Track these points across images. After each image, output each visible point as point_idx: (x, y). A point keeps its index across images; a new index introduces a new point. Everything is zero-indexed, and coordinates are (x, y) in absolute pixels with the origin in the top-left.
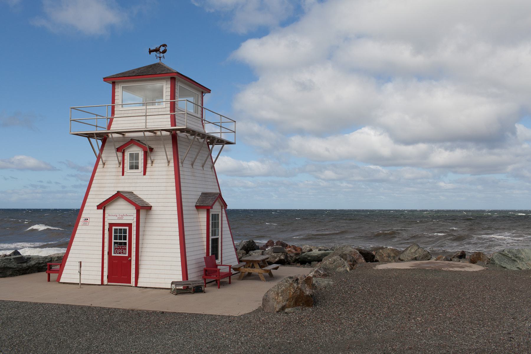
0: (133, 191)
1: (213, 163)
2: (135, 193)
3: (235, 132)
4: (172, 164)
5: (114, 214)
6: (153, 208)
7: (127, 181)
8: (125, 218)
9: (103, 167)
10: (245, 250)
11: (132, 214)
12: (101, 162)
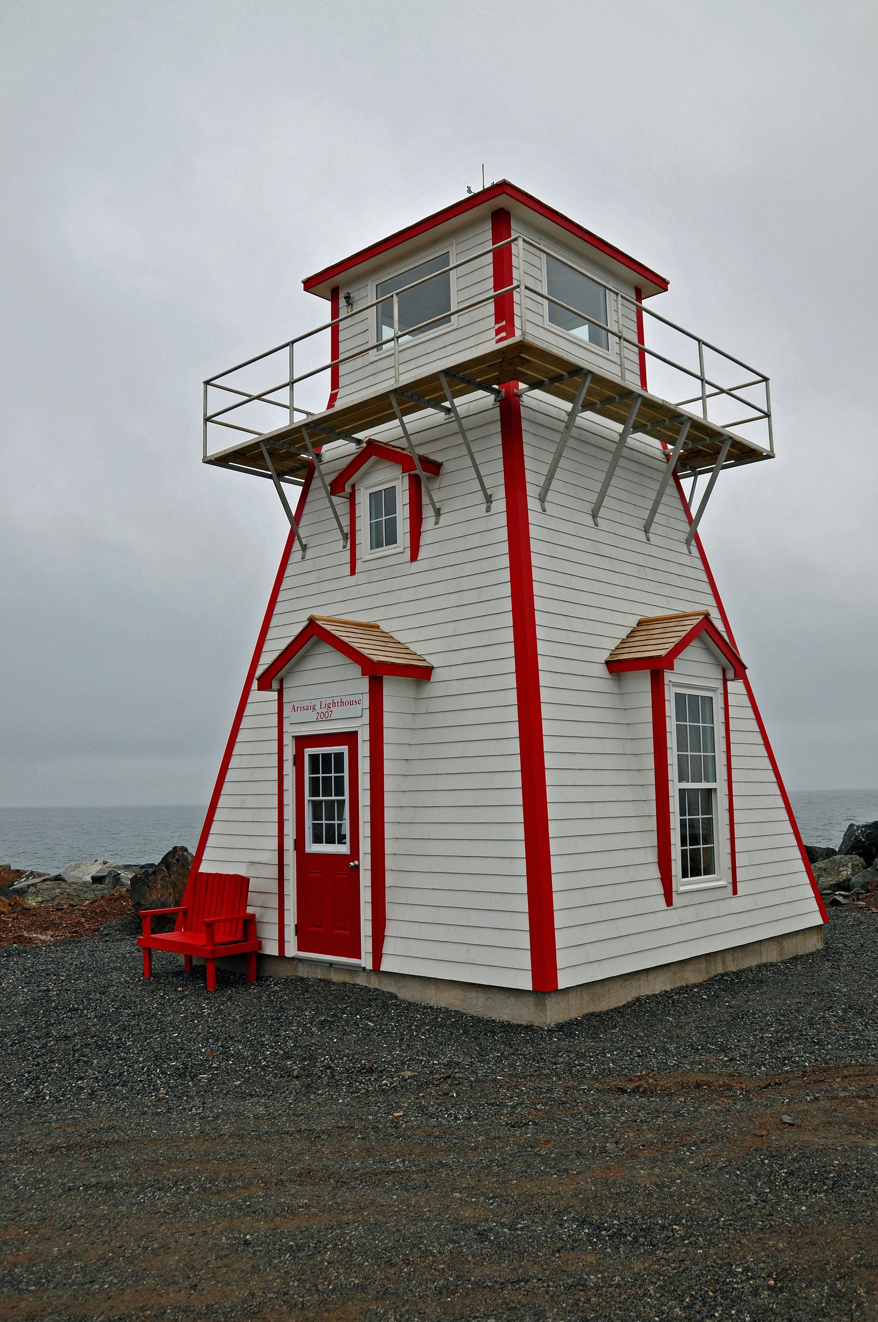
0: (378, 623)
1: (693, 522)
2: (384, 626)
4: (500, 505)
5: (305, 704)
6: (436, 675)
7: (364, 590)
8: (337, 712)
9: (303, 558)
10: (860, 855)
12: (296, 546)
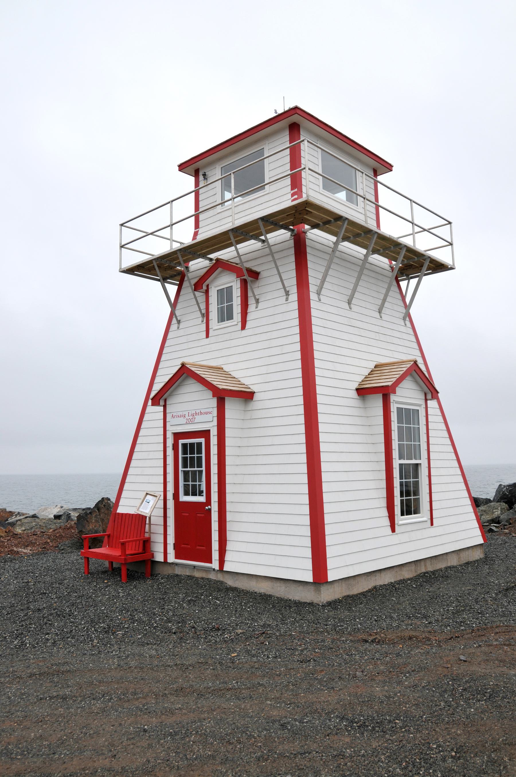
0: (222, 366)
2: (226, 368)
3: (451, 244)
4: (294, 297)
5: (179, 414)
6: (256, 397)
8: (198, 418)
9: (178, 328)
10: (506, 503)
11: (210, 410)
12: (174, 321)
